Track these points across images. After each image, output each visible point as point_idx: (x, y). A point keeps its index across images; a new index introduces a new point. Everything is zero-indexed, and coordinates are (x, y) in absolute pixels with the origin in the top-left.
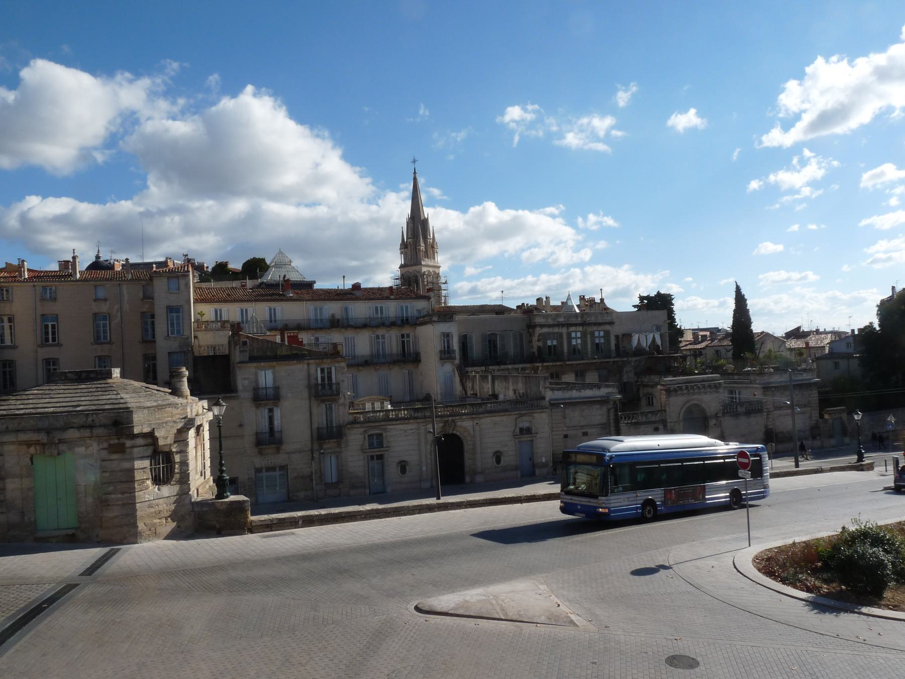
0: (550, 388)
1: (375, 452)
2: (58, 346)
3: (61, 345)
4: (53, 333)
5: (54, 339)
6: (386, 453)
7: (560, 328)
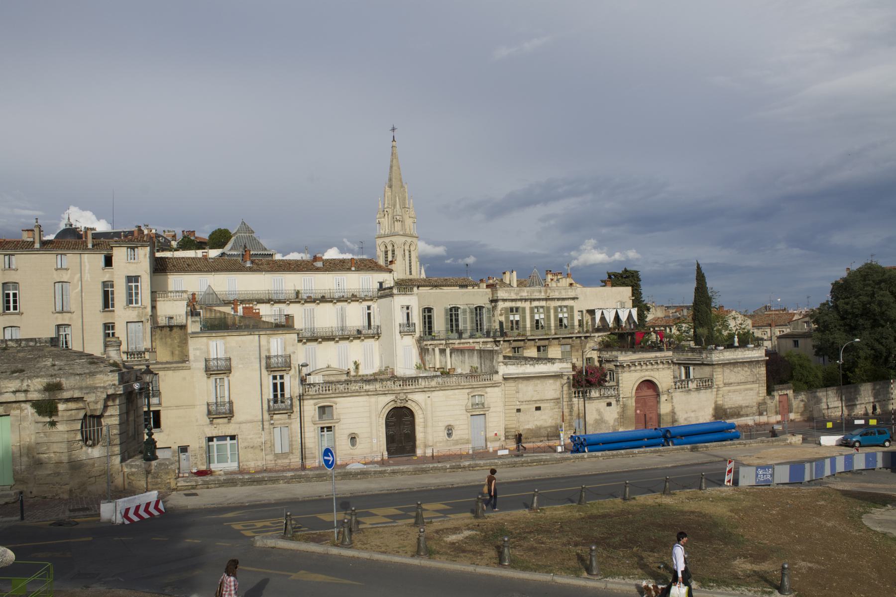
0: (503, 362)
1: (325, 423)
2: (19, 314)
3: (22, 314)
4: (15, 302)
5: (15, 308)
6: (336, 425)
7: (523, 302)
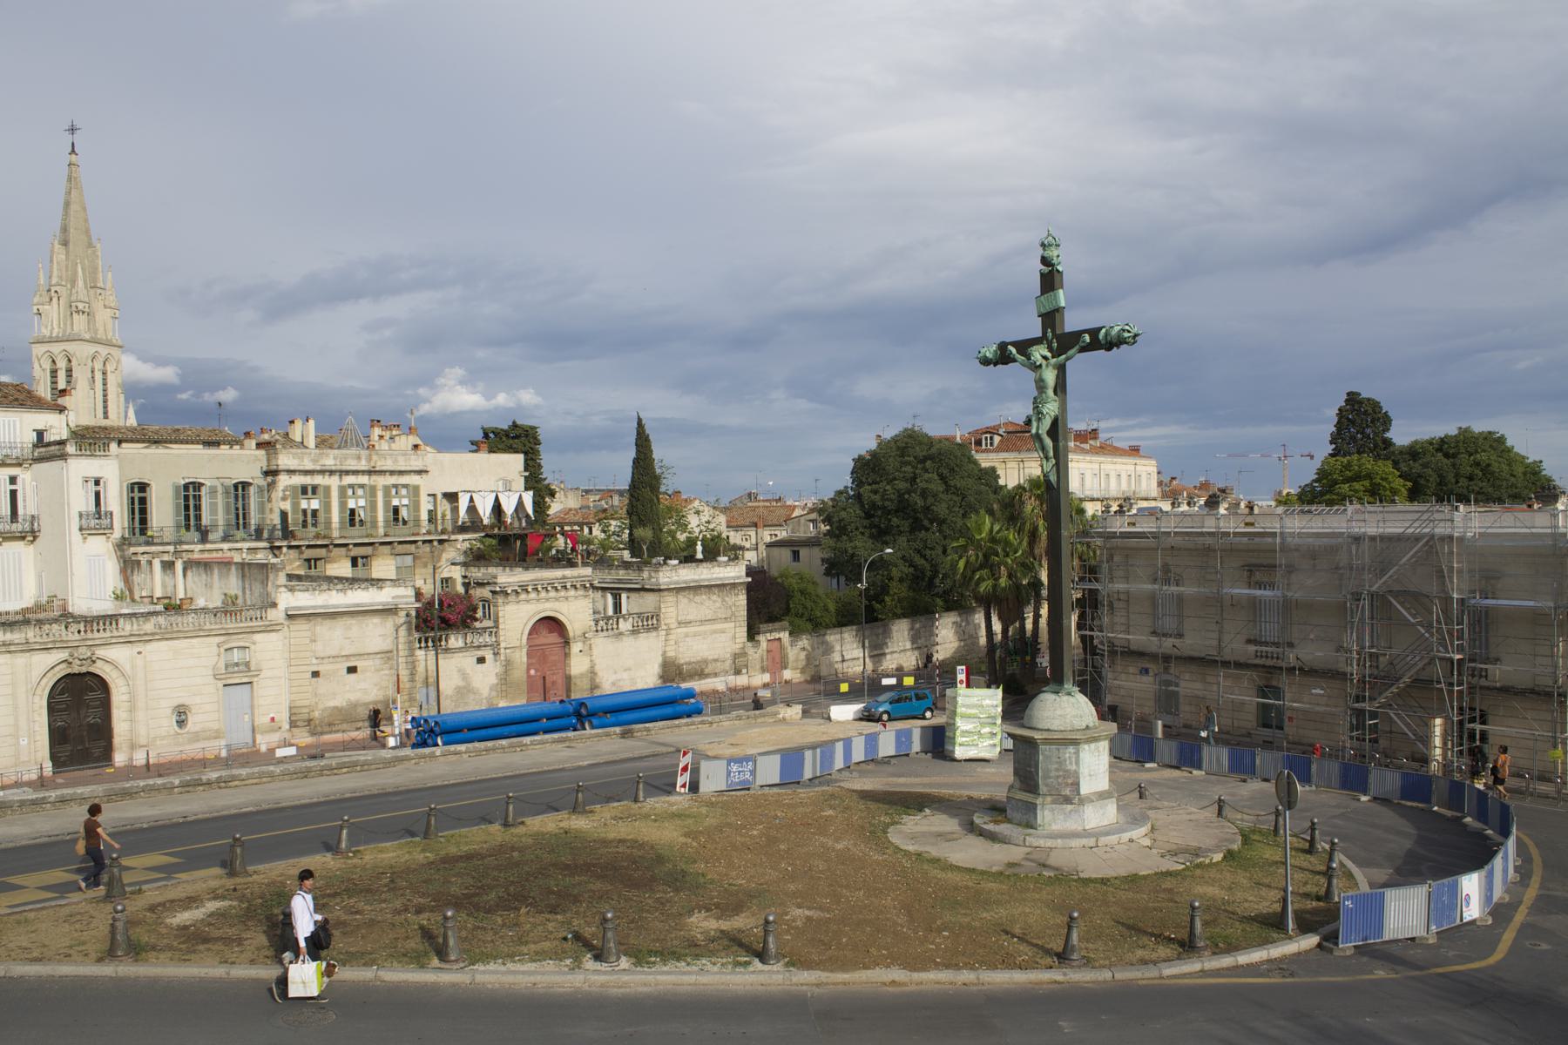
0: (286, 586)
7: (327, 477)
